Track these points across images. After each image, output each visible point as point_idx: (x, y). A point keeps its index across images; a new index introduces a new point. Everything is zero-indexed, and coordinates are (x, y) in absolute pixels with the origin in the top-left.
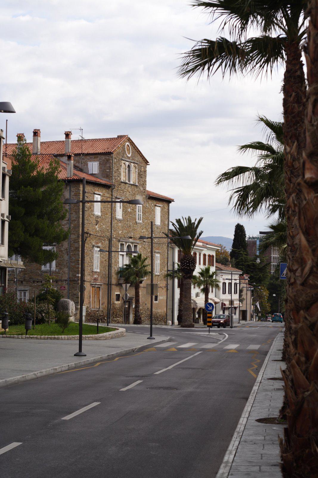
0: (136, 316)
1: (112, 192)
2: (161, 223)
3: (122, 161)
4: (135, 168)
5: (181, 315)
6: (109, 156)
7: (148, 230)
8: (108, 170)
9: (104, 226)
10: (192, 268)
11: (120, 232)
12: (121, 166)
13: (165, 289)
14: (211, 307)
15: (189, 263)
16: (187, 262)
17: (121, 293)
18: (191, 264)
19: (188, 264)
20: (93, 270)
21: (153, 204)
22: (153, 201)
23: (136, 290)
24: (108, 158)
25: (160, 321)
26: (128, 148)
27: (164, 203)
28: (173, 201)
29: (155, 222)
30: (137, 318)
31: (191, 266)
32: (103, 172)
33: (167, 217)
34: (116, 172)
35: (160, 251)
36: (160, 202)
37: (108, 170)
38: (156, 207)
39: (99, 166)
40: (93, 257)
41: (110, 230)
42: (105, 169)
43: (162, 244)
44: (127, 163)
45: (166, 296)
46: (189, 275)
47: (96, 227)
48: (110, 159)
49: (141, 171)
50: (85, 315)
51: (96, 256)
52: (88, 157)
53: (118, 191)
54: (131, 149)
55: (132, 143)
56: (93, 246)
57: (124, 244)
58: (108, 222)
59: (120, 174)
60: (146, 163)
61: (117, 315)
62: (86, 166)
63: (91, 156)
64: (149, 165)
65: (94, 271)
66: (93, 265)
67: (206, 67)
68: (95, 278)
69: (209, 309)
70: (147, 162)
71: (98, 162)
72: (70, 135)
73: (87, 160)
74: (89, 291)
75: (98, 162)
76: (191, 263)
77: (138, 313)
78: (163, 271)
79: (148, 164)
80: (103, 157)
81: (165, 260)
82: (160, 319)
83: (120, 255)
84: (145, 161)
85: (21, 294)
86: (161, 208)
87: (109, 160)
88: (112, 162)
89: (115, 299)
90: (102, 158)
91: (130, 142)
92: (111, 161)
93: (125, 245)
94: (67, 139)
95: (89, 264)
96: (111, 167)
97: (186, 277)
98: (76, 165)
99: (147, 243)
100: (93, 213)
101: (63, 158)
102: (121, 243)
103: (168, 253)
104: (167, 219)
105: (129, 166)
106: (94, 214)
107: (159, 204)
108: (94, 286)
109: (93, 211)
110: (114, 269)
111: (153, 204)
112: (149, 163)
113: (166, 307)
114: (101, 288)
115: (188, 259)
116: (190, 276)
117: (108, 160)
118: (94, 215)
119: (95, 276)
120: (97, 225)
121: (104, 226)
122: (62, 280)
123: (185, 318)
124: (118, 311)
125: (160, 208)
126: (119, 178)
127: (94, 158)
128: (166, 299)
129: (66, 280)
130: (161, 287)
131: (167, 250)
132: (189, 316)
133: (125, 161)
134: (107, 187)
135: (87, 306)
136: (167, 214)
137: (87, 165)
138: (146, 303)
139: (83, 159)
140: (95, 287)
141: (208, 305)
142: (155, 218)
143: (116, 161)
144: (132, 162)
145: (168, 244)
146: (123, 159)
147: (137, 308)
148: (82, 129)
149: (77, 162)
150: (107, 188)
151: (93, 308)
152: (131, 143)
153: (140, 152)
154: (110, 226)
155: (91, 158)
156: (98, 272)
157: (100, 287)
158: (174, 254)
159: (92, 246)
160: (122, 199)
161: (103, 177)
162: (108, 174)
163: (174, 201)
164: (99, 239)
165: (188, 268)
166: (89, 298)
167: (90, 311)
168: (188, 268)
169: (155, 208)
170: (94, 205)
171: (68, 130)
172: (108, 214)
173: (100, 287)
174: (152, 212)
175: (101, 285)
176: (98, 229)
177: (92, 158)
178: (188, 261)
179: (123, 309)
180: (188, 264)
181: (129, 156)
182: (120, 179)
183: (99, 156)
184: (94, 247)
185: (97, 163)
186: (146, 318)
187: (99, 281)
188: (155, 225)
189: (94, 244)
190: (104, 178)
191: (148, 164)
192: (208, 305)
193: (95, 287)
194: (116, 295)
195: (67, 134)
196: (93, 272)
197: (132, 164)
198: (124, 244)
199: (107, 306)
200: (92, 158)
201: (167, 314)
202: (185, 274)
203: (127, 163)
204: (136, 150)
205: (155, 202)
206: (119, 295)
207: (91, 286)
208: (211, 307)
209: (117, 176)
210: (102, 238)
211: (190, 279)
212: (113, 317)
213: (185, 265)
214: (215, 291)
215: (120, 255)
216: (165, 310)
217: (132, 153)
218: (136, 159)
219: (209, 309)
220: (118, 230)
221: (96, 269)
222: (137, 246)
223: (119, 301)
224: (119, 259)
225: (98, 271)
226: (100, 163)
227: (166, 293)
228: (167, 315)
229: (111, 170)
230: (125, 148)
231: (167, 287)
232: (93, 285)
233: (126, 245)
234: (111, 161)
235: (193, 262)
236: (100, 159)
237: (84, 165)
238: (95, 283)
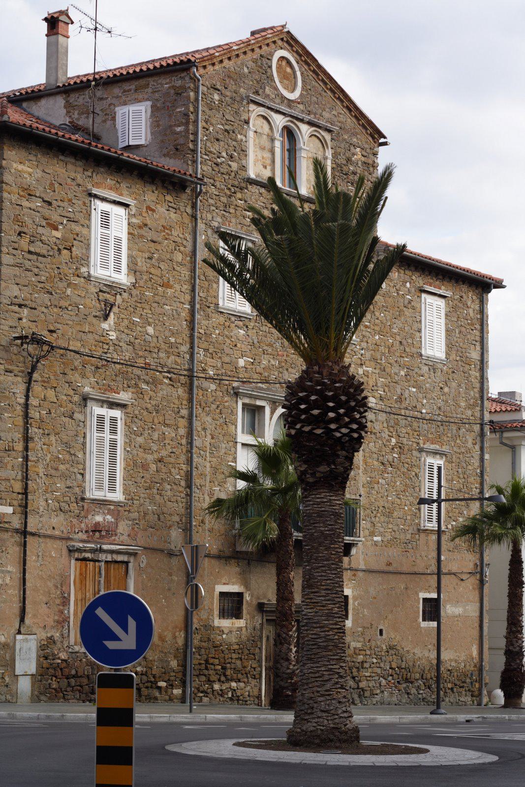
0: (277, 676)
1: (194, 206)
2: (447, 354)
3: (252, 107)
4: (320, 145)
5: (515, 669)
6: (182, 75)
7: (388, 370)
8: (179, 129)
10: (337, 430)
11: (241, 362)
12: (247, 122)
13: (473, 581)
14: (125, 629)
15: (321, 404)
16: (313, 398)
17: (247, 587)
18: (332, 409)
19: (316, 412)
20: (83, 492)
21: (408, 285)
22: (408, 273)
23: (278, 575)
24: (179, 83)
25: (452, 689)
26: (289, 70)
27: (464, 288)
29: (420, 348)
30: (282, 683)
31: (332, 421)
32: (165, 135)
33: (478, 338)
34: (218, 140)
35: (445, 449)
36: (445, 283)
37: (179, 129)
38: (424, 295)
39: (151, 116)
40: (84, 444)
41: (185, 348)
42: (171, 126)
43: (454, 427)
44: (279, 121)
45: (478, 604)
46: (323, 468)
47: (105, 325)
48: (187, 85)
49: (349, 160)
50: (32, 669)
51: (101, 440)
52: (116, 90)
53: (232, 211)
54: (303, 81)
55: (306, 57)
56: (85, 399)
57: (264, 407)
58: (175, 315)
59: (244, 152)
60: (373, 138)
61: (228, 672)
62: (109, 123)
63: (126, 86)
64: (385, 144)
65: (88, 495)
66: (82, 475)
68: (98, 524)
69: (111, 645)
70: (376, 135)
71: (149, 103)
72: (61, 24)
73: (114, 101)
74: (61, 576)
75: (149, 103)
76: (331, 404)
77: (285, 664)
79: (382, 140)
80: (165, 84)
81: (471, 479)
82: (450, 686)
84: (370, 130)
86: (447, 304)
87: (185, 89)
88: (197, 100)
89: (216, 612)
90: (162, 84)
91: (297, 52)
92: (192, 94)
93: (268, 410)
94: (53, 38)
95: (62, 467)
96: (192, 117)
97: (311, 480)
98: (80, 123)
99: (384, 415)
100: (84, 270)
101: (39, 104)
102: (247, 401)
103: (482, 459)
104: (478, 344)
105: (290, 134)
106: (89, 275)
107: (440, 288)
108: (88, 555)
109: (85, 260)
110: (203, 500)
111: (408, 285)
112: (385, 137)
113: (477, 642)
114: (131, 565)
115: (318, 383)
116: (331, 471)
117: (179, 92)
118: (88, 278)
119: (99, 518)
120: (106, 317)
121: (150, 330)
123: (308, 694)
124: (234, 656)
125: (443, 300)
126: (234, 166)
127: (136, 90)
128: (477, 614)
130: (454, 574)
131: (477, 447)
132: (328, 686)
133: (269, 108)
134: (163, 182)
135: (43, 635)
136: (478, 327)
137: (114, 119)
138: (381, 627)
139: (101, 99)
140: (99, 561)
141: (100, 612)
142: (420, 331)
143: (221, 101)
144: (302, 121)
145: (482, 429)
146: (259, 99)
147: (281, 643)
149: (83, 113)
150: (164, 187)
152: (300, 55)
153: (342, 91)
154: (187, 332)
155: (125, 91)
156: (117, 504)
157: (127, 563)
158: (517, 467)
159: (76, 398)
160: (253, 242)
161: (164, 155)
162: (181, 141)
163: (504, 287)
164: (121, 372)
165: (319, 431)
166: (58, 601)
167: (63, 656)
168: (319, 431)
169: (420, 297)
170: (89, 240)
171: (53, 9)
172: (171, 287)
173: (127, 563)
174: (408, 312)
175: (135, 554)
176: (113, 336)
177: (129, 90)
178: (317, 393)
179: (260, 649)
180: (316, 412)
181: (294, 96)
182: (244, 168)
183: (151, 81)
184: (90, 404)
185: (143, 108)
186: (384, 682)
187: (125, 538)
188: (421, 355)
189: (87, 389)
190: (168, 159)
191: (382, 140)
192: (100, 612)
193: (99, 561)
194: (222, 594)
195: (52, 17)
196: (83, 499)
197: (304, 128)
198: (264, 407)
199: (436, 645)
200: (129, 90)
201: (481, 665)
202: (305, 462)
203: (279, 121)
204: (325, 84)
205: (419, 280)
206: (240, 595)
207: (70, 556)
208: (125, 629)
209: (224, 154)
210: (137, 372)
211: (465, 525)
212: (203, 678)
213: (303, 417)
215: (239, 446)
216: (475, 653)
217: (303, 89)
218: (326, 115)
219: (111, 645)
220: (227, 350)
221: (100, 487)
223: (242, 618)
225: (118, 496)
226: (156, 106)
227: (477, 593)
228: (481, 670)
229: (191, 127)
230: (270, 67)
231: (482, 573)
232: (79, 550)
233: (272, 413)
234: (192, 94)
235: (343, 398)
236: (154, 92)
237: (105, 121)
238: (96, 543)
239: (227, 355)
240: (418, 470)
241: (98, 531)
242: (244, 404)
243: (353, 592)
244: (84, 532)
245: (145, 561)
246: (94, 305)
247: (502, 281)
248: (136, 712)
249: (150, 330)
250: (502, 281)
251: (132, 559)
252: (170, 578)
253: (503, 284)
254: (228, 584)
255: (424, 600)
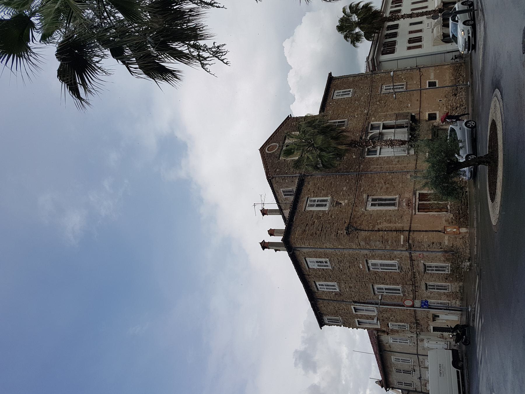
9: (345, 188)
28: (330, 74)
37: (287, 181)
64: (291, 115)
67: (205, 62)
78: (403, 77)
79: (290, 116)
83: (380, 156)
85: (428, 270)
112: (289, 115)
122: (411, 256)
129: (410, 253)
148: (254, 204)
151: (449, 272)
177: (278, 194)
191: (290, 116)
214: (421, 6)
215: (380, 156)
222: (372, 125)
224: (385, 157)
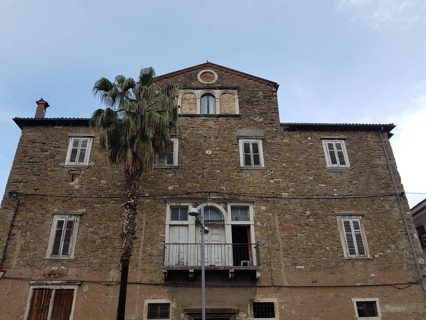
153: (244, 74)
206: (168, 305)
239: (160, 186)
240: (336, 226)
241: (53, 274)
242: (171, 207)
243: (278, 300)
244: (42, 275)
245: (87, 289)
246: (66, 175)
247: (393, 124)
248: (235, 114)
249: (103, 182)
250: (393, 124)
251: (76, 288)
252: (107, 296)
253: (49, 104)
254: (156, 299)
255: (357, 303)
